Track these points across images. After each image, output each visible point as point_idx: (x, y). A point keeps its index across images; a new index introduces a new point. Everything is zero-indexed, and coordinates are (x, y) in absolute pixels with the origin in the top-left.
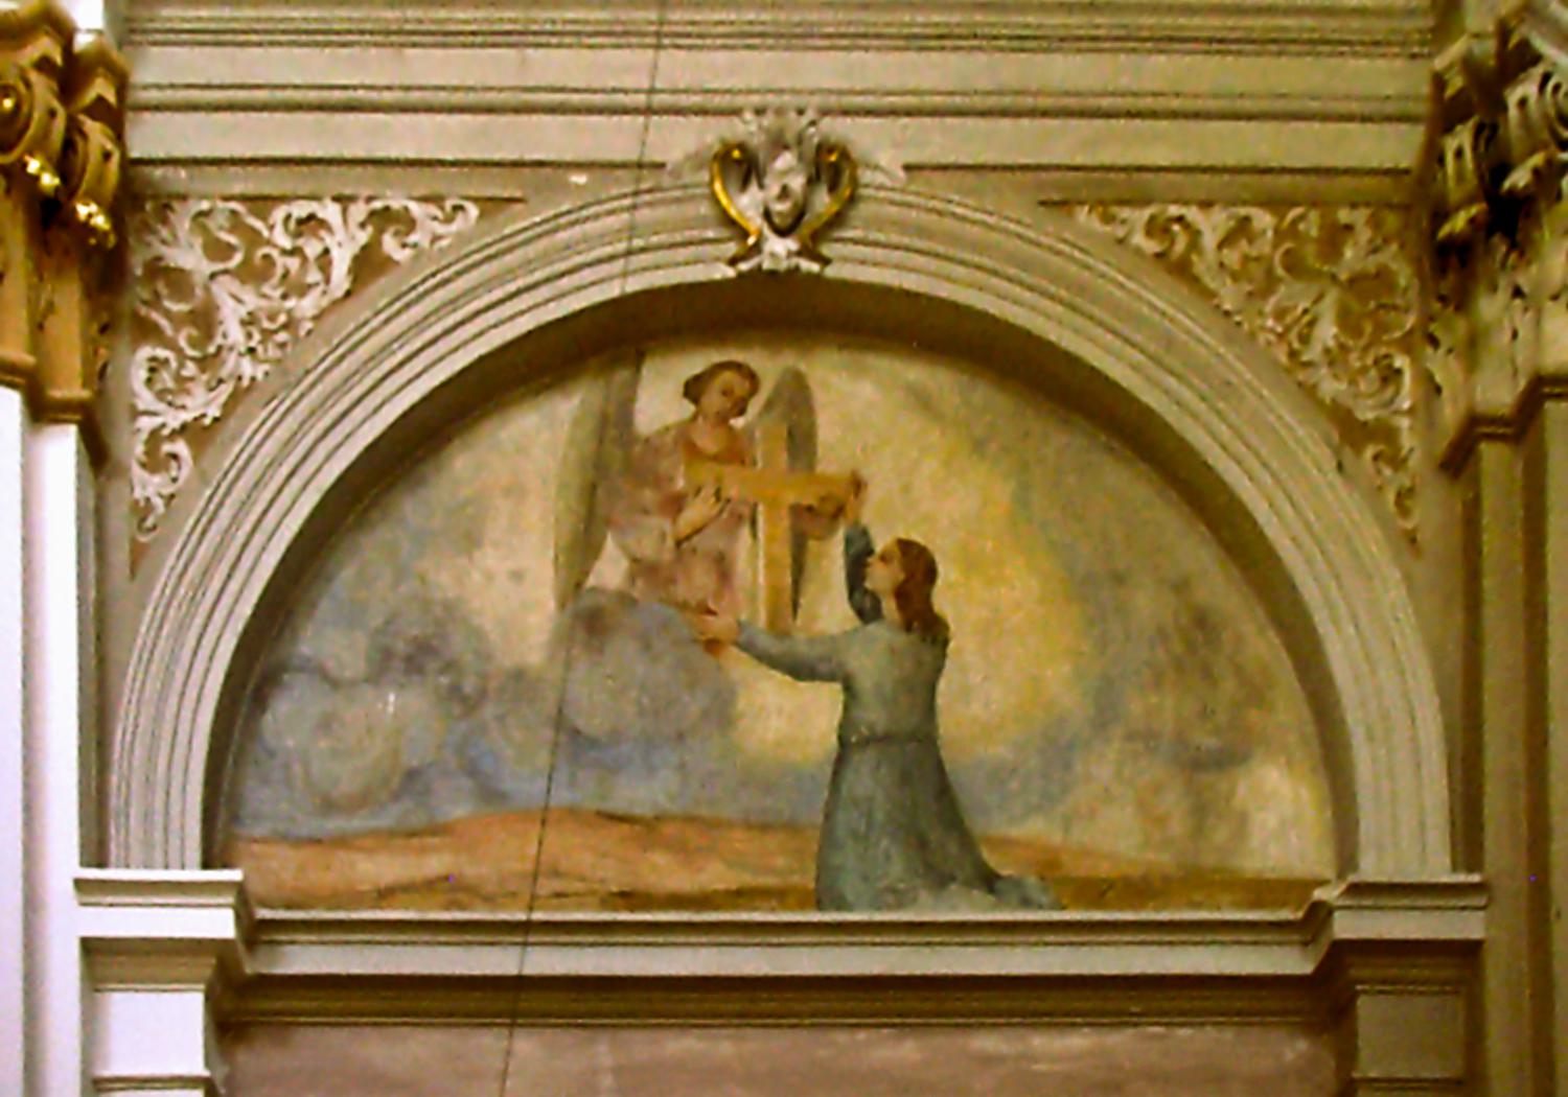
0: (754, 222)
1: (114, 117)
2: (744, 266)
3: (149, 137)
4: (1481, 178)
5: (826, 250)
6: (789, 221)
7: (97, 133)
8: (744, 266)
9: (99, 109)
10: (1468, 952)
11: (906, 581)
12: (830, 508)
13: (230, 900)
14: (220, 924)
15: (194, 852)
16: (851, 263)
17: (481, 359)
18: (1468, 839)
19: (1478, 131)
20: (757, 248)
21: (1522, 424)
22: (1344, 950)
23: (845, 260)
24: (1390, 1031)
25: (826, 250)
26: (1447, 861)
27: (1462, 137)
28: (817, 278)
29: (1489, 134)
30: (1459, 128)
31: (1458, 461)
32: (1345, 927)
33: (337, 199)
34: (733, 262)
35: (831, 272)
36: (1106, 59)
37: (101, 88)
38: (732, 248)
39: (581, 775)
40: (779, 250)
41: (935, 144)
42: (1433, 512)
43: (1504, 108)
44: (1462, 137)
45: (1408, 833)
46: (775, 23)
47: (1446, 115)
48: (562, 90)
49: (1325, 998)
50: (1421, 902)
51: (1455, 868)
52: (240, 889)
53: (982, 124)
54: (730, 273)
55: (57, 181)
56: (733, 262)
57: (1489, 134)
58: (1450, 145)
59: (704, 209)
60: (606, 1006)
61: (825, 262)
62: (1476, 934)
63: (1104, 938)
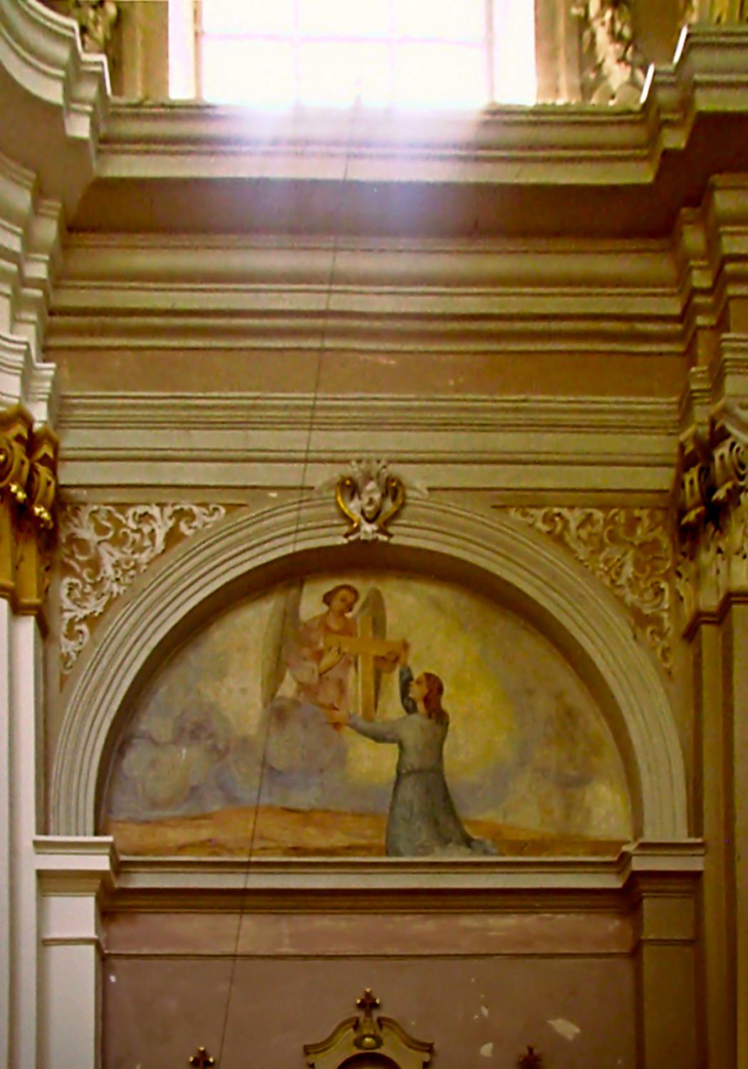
0: (357, 516)
1: (52, 464)
2: (352, 538)
3: (69, 474)
5: (391, 530)
7: (43, 471)
8: (352, 538)
9: (45, 460)
10: (696, 876)
13: (107, 850)
14: (102, 863)
16: (402, 536)
18: (696, 825)
20: (357, 529)
21: (721, 616)
25: (391, 530)
27: (693, 474)
28: (386, 544)
29: (706, 472)
31: (691, 634)
32: (638, 864)
33: (158, 504)
34: (346, 536)
35: (393, 541)
37: (46, 450)
38: (346, 529)
43: (713, 459)
44: (693, 474)
47: (686, 463)
49: (627, 900)
50: (523, 870)
51: (38, 833)
52: (112, 846)
54: (345, 541)
56: (346, 536)
57: (706, 472)
58: (687, 478)
59: (333, 510)
61: (390, 535)
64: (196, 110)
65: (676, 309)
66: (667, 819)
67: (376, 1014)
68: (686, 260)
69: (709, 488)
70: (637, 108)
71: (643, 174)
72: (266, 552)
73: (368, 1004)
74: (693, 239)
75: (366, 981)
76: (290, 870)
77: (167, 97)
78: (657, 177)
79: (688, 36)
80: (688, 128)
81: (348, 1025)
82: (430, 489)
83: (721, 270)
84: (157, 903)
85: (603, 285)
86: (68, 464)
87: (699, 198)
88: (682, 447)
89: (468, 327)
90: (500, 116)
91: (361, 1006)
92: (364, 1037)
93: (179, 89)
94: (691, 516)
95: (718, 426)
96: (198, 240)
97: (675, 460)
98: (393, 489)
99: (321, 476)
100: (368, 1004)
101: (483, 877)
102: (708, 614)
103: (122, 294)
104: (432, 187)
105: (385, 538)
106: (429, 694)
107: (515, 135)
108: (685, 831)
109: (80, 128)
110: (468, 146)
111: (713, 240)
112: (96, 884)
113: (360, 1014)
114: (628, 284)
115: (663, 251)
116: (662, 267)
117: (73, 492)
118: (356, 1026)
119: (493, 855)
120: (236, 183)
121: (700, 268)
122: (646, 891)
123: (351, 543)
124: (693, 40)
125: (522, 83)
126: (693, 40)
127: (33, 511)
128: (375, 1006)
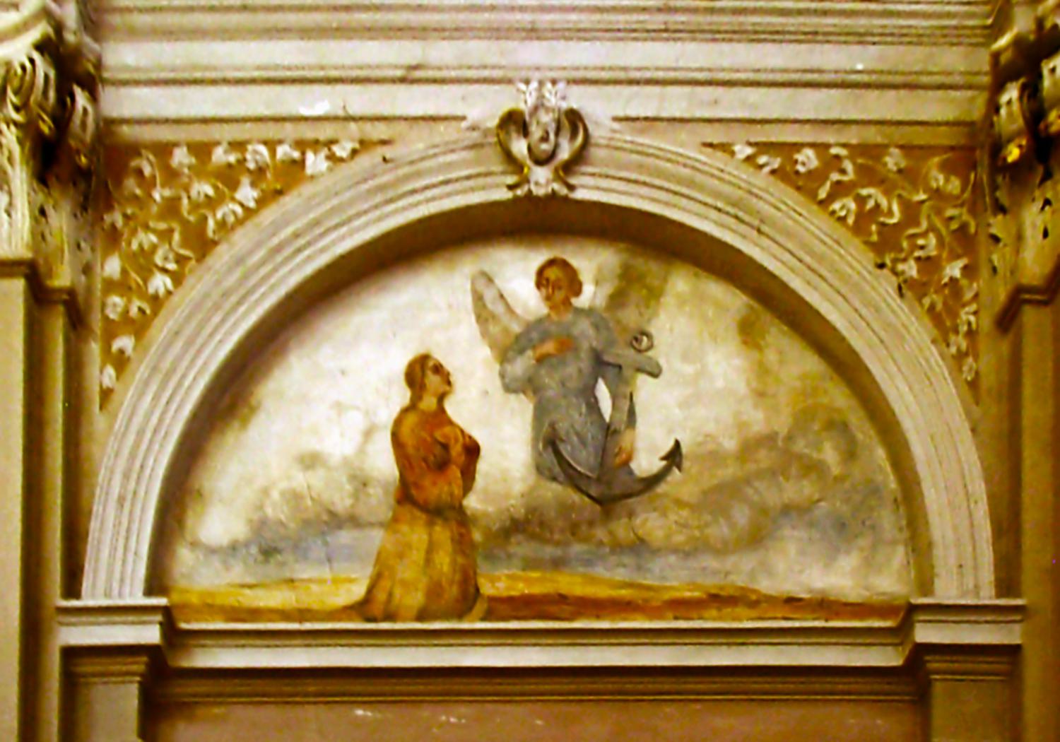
1: (91, 85)
2: (519, 192)
3: (122, 103)
7: (81, 99)
8: (519, 192)
10: (1013, 651)
13: (159, 618)
14: (150, 634)
16: (587, 190)
18: (1007, 582)
19: (1023, 89)
23: (583, 186)
24: (957, 716)
26: (993, 592)
27: (1012, 93)
28: (566, 199)
29: (1032, 90)
31: (1007, 320)
32: (925, 634)
33: (265, 143)
34: (511, 187)
35: (580, 195)
36: (725, 47)
38: (511, 180)
39: (449, 499)
40: (542, 180)
41: (663, 112)
43: (1040, 76)
44: (1012, 93)
45: (963, 564)
49: (914, 679)
51: (999, 595)
52: (166, 611)
54: (508, 195)
55: (1010, 159)
56: (511, 188)
57: (1032, 90)
58: (1004, 99)
61: (572, 188)
62: (1016, 640)
72: (387, 216)
76: (518, 641)
82: (617, 119)
86: (124, 91)
88: (996, 56)
95: (1048, 24)
101: (506, 651)
105: (564, 191)
106: (540, 413)
112: (139, 665)
119: (404, 620)
122: (937, 672)
123: (516, 200)
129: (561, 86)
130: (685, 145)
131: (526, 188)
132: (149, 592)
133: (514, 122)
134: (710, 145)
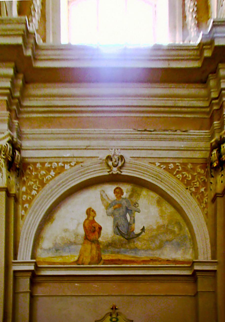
2: (110, 173)
3: (26, 154)
4: (217, 157)
5: (122, 170)
6: (115, 165)
7: (17, 153)
8: (110, 173)
10: (215, 271)
11: (115, 220)
12: (108, 208)
13: (34, 264)
14: (32, 268)
15: (30, 257)
16: (125, 172)
17: (157, 186)
22: (196, 271)
25: (122, 170)
27: (215, 152)
28: (120, 174)
29: (219, 151)
30: (214, 150)
31: (214, 200)
32: (196, 268)
35: (123, 174)
38: (109, 170)
42: (210, 209)
44: (215, 152)
46: (146, 137)
47: (212, 149)
48: (143, 147)
49: (194, 277)
50: (130, 269)
52: (35, 263)
53: (146, 151)
54: (108, 174)
56: (108, 172)
57: (219, 151)
58: (213, 153)
60: (64, 279)
61: (121, 172)
62: (215, 269)
63: (157, 269)
64: (69, 48)
65: (206, 104)
66: (204, 253)
67: (117, 311)
68: (210, 89)
69: (220, 156)
70: (197, 45)
71: (196, 64)
73: (114, 308)
74: (212, 83)
75: (114, 301)
77: (61, 43)
78: (203, 65)
79: (213, 22)
80: (213, 50)
81: (108, 315)
83: (220, 92)
84: (61, 279)
85: (186, 98)
86: (26, 151)
87: (215, 71)
89: (157, 109)
90: (157, 48)
91: (112, 309)
92: (113, 318)
93: (64, 41)
94: (215, 165)
96: (68, 85)
97: (209, 149)
98: (122, 158)
99: (103, 155)
100: (114, 308)
101: (107, 271)
102: (218, 194)
103: (67, 101)
104: (138, 69)
105: (120, 173)
107: (160, 53)
108: (211, 259)
109: (29, 53)
110: (151, 56)
111: (219, 84)
113: (111, 311)
114: (189, 96)
115: (203, 88)
116: (203, 92)
117: (27, 159)
118: (111, 315)
120: (79, 68)
121: (213, 91)
122: (199, 276)
123: (110, 175)
124: (214, 23)
125: (165, 37)
126: (214, 23)
127: (218, 162)
128: (116, 309)
129: (119, 150)
130: (145, 163)
131: (112, 172)
132: (32, 259)
133: (109, 158)
134: (151, 163)
